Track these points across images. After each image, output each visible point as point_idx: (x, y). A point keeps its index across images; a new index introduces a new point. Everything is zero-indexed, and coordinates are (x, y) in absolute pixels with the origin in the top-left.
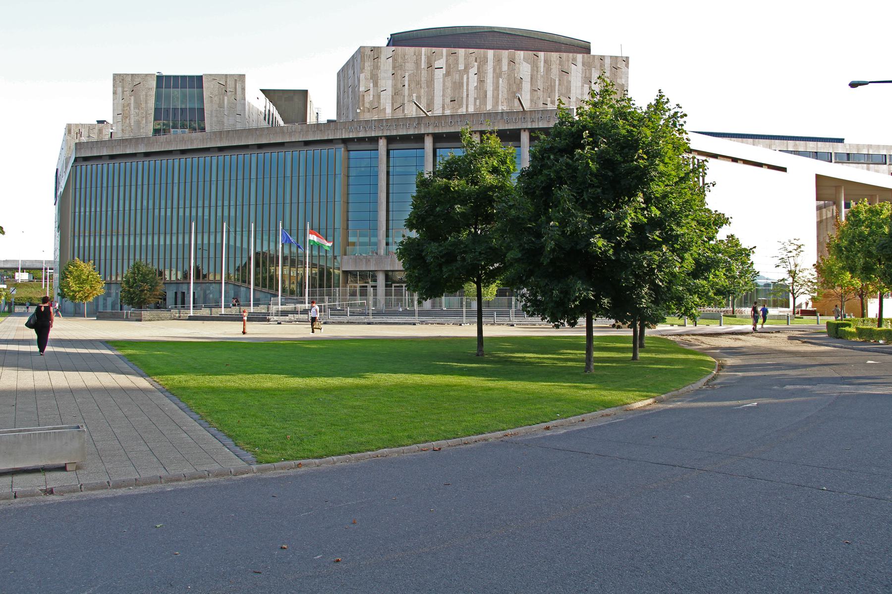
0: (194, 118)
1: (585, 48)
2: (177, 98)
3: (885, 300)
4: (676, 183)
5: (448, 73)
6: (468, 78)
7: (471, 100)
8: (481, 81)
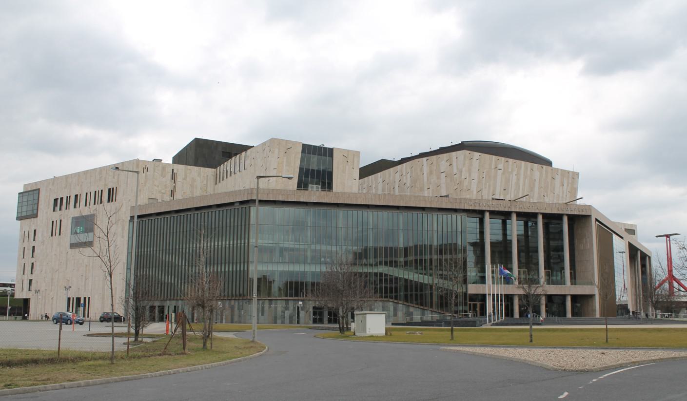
0: (325, 180)
1: (548, 163)
2: (314, 163)
3: (111, 350)
4: (48, 208)
5: (503, 173)
6: (512, 176)
7: (513, 190)
8: (518, 179)
